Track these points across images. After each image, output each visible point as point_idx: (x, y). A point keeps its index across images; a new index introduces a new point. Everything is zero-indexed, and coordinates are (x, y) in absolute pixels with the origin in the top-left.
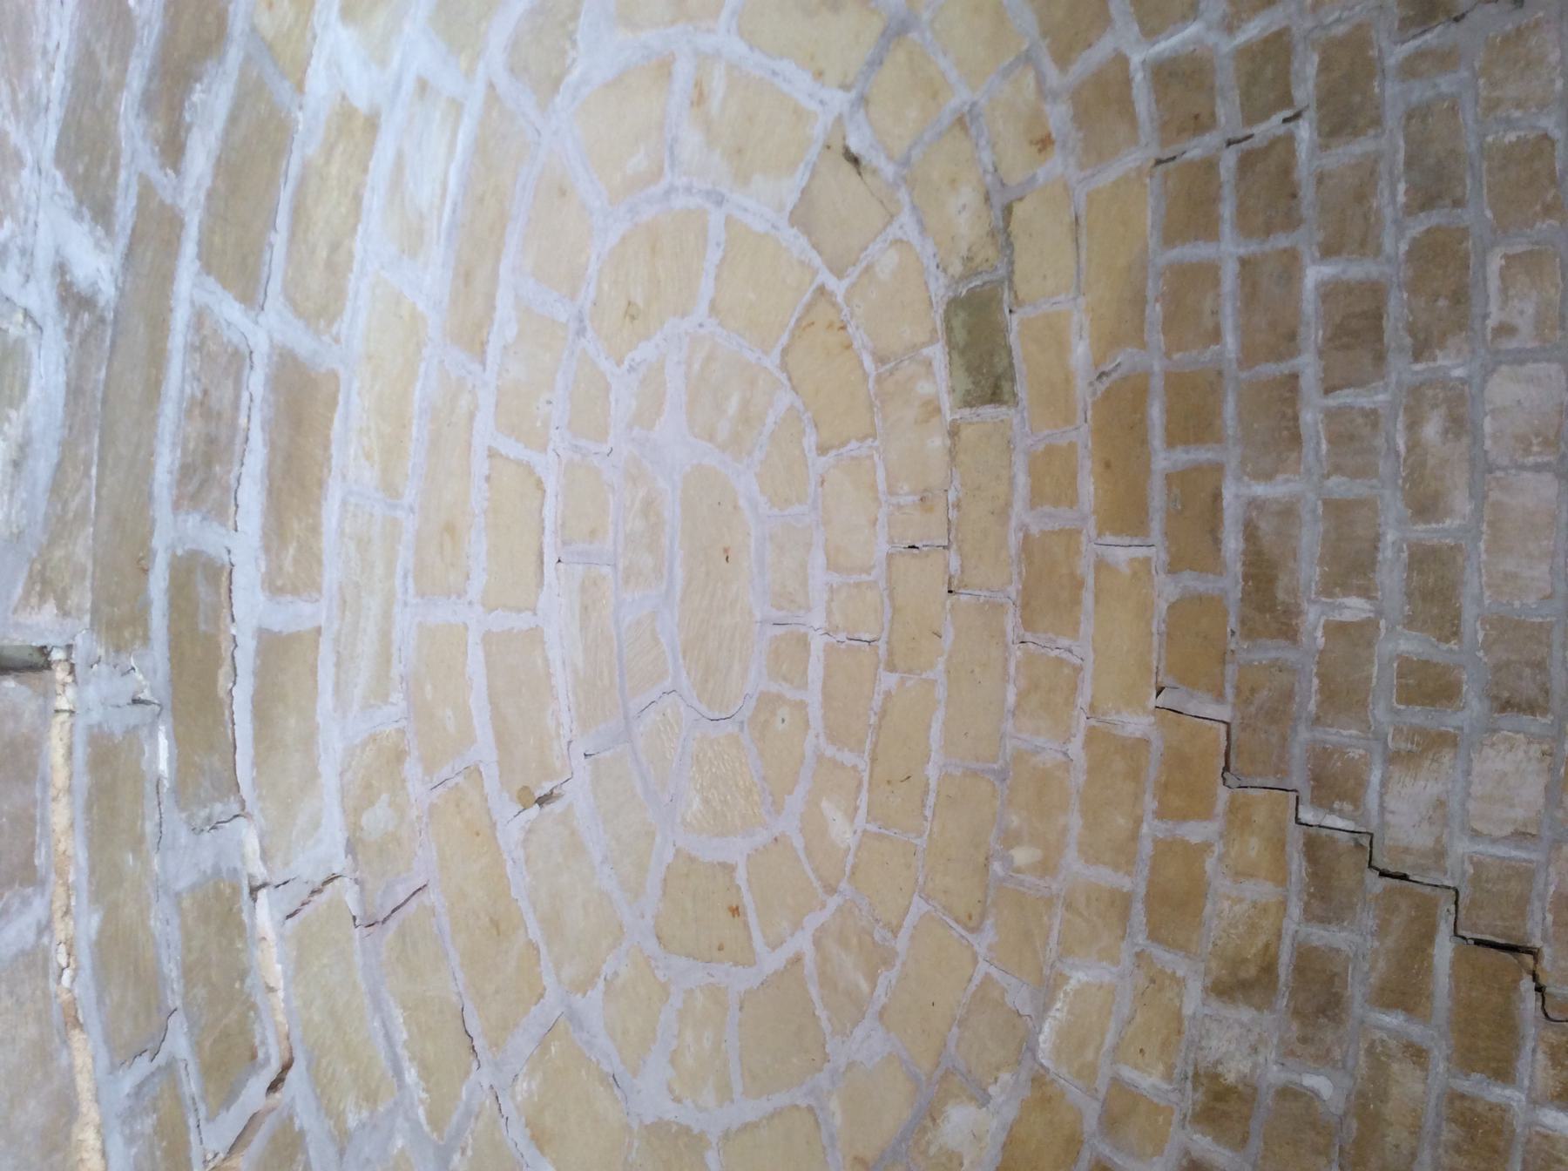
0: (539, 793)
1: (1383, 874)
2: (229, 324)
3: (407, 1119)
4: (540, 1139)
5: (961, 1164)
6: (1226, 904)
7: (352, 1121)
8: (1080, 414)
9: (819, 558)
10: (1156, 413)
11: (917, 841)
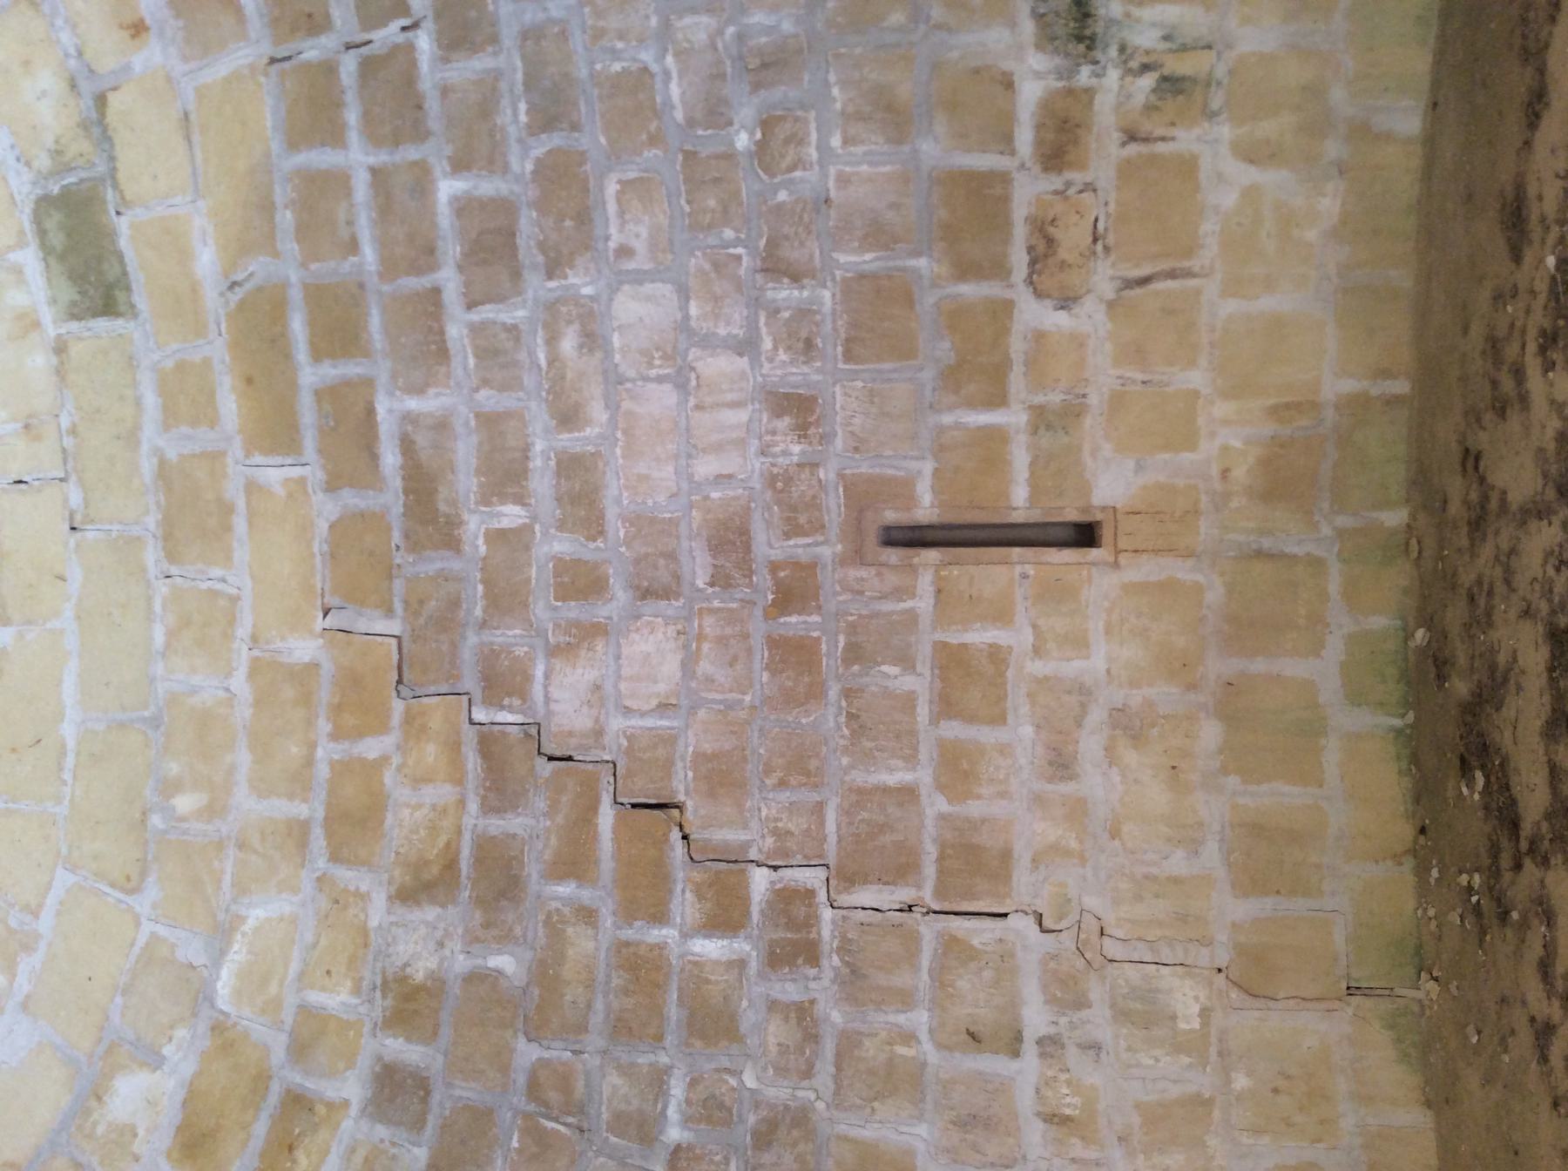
1: (551, 758)
5: (135, 1135)
6: (407, 812)
8: (213, 327)
10: (298, 325)
11: (57, 810)
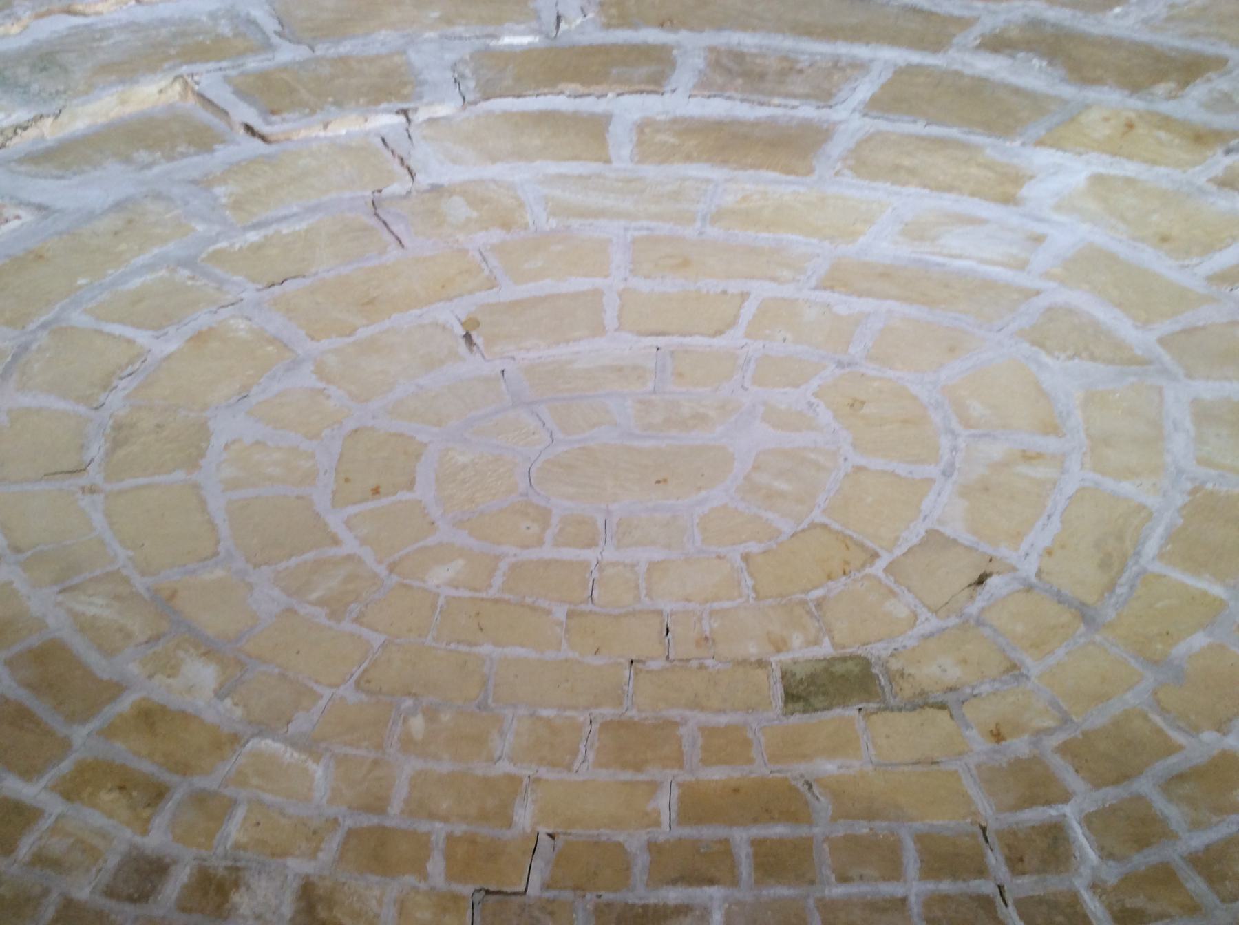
0: (474, 334)
2: (855, 89)
3: (218, 234)
4: (199, 338)
5: (169, 676)
7: (219, 190)
9: (657, 555)
10: (779, 830)
